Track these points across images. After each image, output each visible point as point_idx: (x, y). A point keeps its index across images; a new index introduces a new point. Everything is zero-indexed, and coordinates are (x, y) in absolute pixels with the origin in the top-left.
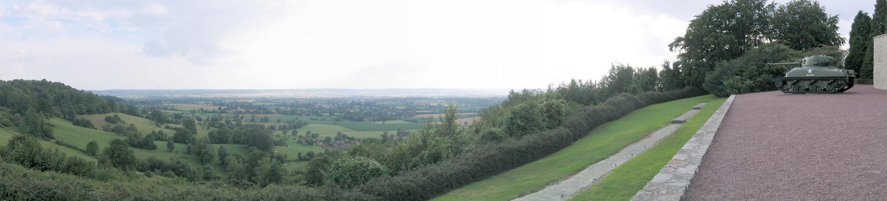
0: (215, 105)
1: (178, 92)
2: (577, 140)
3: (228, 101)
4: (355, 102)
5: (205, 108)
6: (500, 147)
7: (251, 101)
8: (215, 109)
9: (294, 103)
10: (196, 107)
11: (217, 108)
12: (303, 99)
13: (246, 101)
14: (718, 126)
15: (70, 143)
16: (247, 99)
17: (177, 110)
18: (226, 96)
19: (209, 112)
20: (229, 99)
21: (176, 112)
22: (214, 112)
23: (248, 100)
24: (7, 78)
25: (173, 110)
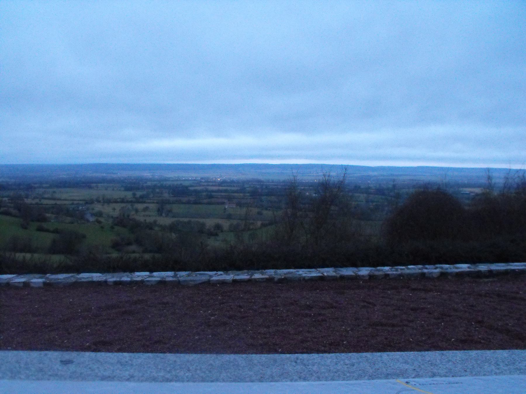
0: (127, 189)
1: (63, 168)
2: (263, 382)
3: (149, 183)
4: (359, 187)
5: (109, 194)
6: (407, 361)
7: (187, 184)
8: (126, 196)
9: (258, 187)
10: (93, 193)
11: (129, 195)
12: (273, 182)
13: (179, 183)
14: (237, 383)
15: (142, 275)
16: (180, 180)
17: (59, 199)
18: (147, 174)
19: (116, 202)
20: (150, 180)
21: (59, 202)
22: (123, 201)
23: (182, 182)
24: (3, 163)
25: (54, 199)
